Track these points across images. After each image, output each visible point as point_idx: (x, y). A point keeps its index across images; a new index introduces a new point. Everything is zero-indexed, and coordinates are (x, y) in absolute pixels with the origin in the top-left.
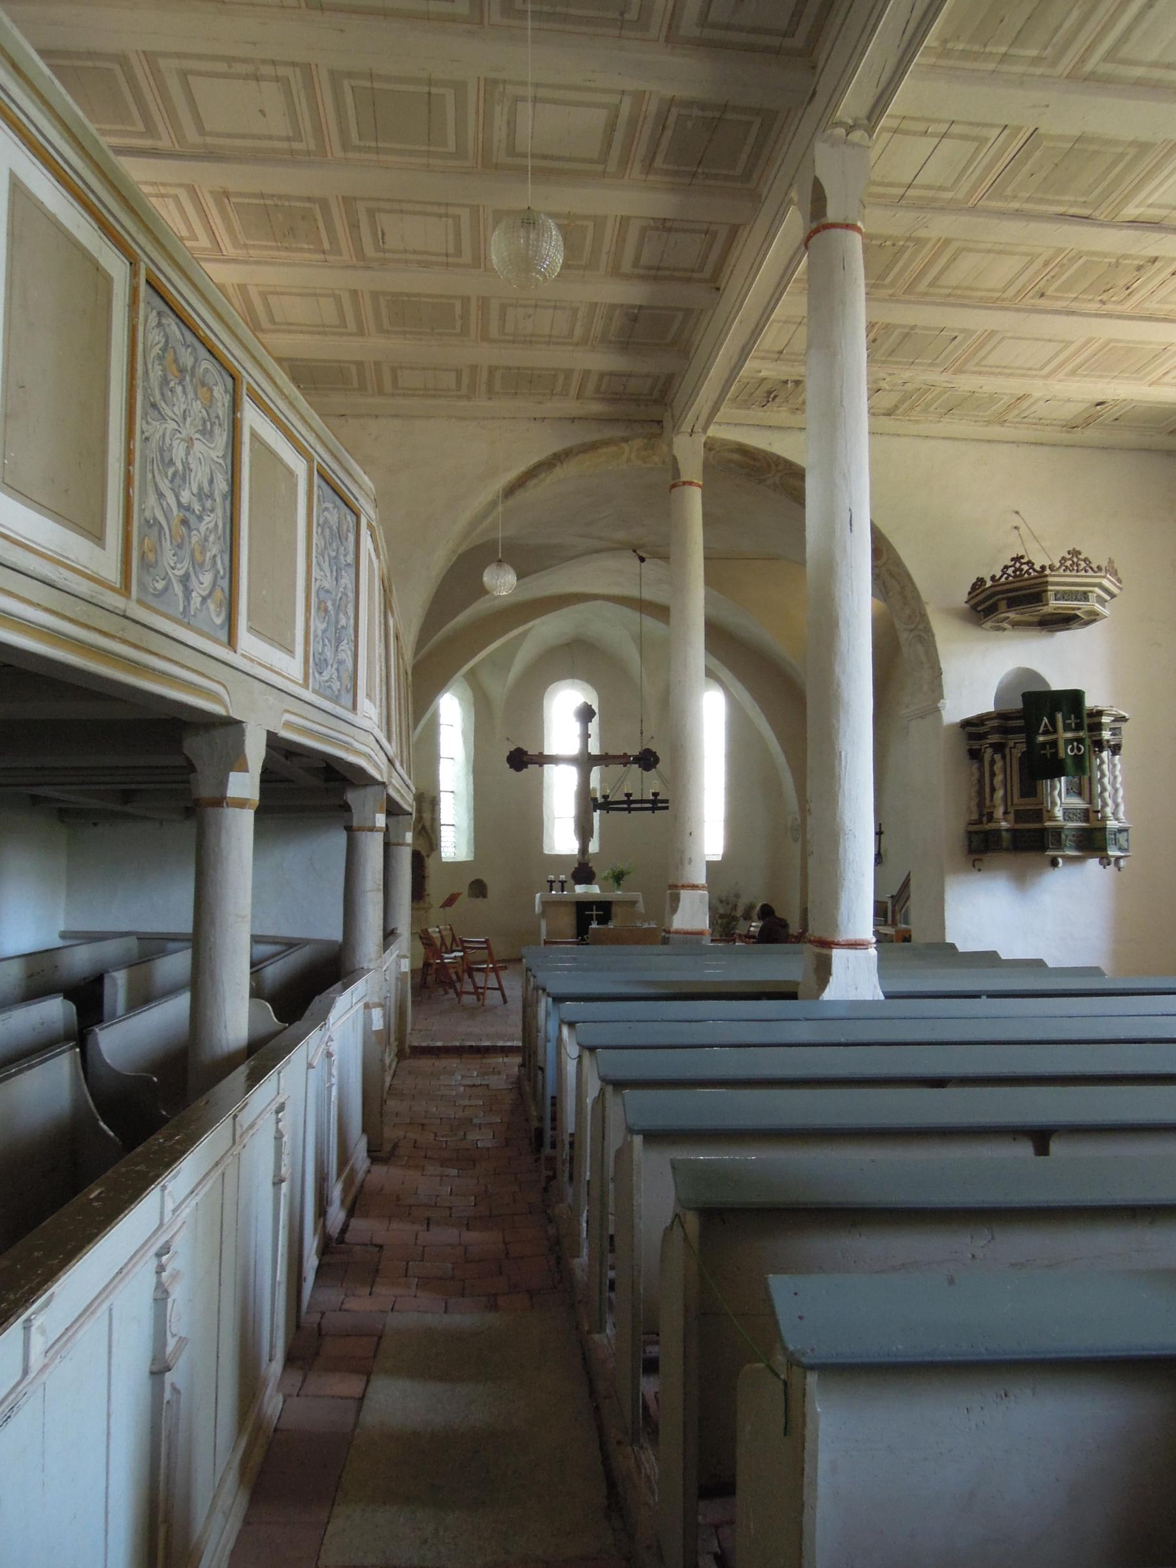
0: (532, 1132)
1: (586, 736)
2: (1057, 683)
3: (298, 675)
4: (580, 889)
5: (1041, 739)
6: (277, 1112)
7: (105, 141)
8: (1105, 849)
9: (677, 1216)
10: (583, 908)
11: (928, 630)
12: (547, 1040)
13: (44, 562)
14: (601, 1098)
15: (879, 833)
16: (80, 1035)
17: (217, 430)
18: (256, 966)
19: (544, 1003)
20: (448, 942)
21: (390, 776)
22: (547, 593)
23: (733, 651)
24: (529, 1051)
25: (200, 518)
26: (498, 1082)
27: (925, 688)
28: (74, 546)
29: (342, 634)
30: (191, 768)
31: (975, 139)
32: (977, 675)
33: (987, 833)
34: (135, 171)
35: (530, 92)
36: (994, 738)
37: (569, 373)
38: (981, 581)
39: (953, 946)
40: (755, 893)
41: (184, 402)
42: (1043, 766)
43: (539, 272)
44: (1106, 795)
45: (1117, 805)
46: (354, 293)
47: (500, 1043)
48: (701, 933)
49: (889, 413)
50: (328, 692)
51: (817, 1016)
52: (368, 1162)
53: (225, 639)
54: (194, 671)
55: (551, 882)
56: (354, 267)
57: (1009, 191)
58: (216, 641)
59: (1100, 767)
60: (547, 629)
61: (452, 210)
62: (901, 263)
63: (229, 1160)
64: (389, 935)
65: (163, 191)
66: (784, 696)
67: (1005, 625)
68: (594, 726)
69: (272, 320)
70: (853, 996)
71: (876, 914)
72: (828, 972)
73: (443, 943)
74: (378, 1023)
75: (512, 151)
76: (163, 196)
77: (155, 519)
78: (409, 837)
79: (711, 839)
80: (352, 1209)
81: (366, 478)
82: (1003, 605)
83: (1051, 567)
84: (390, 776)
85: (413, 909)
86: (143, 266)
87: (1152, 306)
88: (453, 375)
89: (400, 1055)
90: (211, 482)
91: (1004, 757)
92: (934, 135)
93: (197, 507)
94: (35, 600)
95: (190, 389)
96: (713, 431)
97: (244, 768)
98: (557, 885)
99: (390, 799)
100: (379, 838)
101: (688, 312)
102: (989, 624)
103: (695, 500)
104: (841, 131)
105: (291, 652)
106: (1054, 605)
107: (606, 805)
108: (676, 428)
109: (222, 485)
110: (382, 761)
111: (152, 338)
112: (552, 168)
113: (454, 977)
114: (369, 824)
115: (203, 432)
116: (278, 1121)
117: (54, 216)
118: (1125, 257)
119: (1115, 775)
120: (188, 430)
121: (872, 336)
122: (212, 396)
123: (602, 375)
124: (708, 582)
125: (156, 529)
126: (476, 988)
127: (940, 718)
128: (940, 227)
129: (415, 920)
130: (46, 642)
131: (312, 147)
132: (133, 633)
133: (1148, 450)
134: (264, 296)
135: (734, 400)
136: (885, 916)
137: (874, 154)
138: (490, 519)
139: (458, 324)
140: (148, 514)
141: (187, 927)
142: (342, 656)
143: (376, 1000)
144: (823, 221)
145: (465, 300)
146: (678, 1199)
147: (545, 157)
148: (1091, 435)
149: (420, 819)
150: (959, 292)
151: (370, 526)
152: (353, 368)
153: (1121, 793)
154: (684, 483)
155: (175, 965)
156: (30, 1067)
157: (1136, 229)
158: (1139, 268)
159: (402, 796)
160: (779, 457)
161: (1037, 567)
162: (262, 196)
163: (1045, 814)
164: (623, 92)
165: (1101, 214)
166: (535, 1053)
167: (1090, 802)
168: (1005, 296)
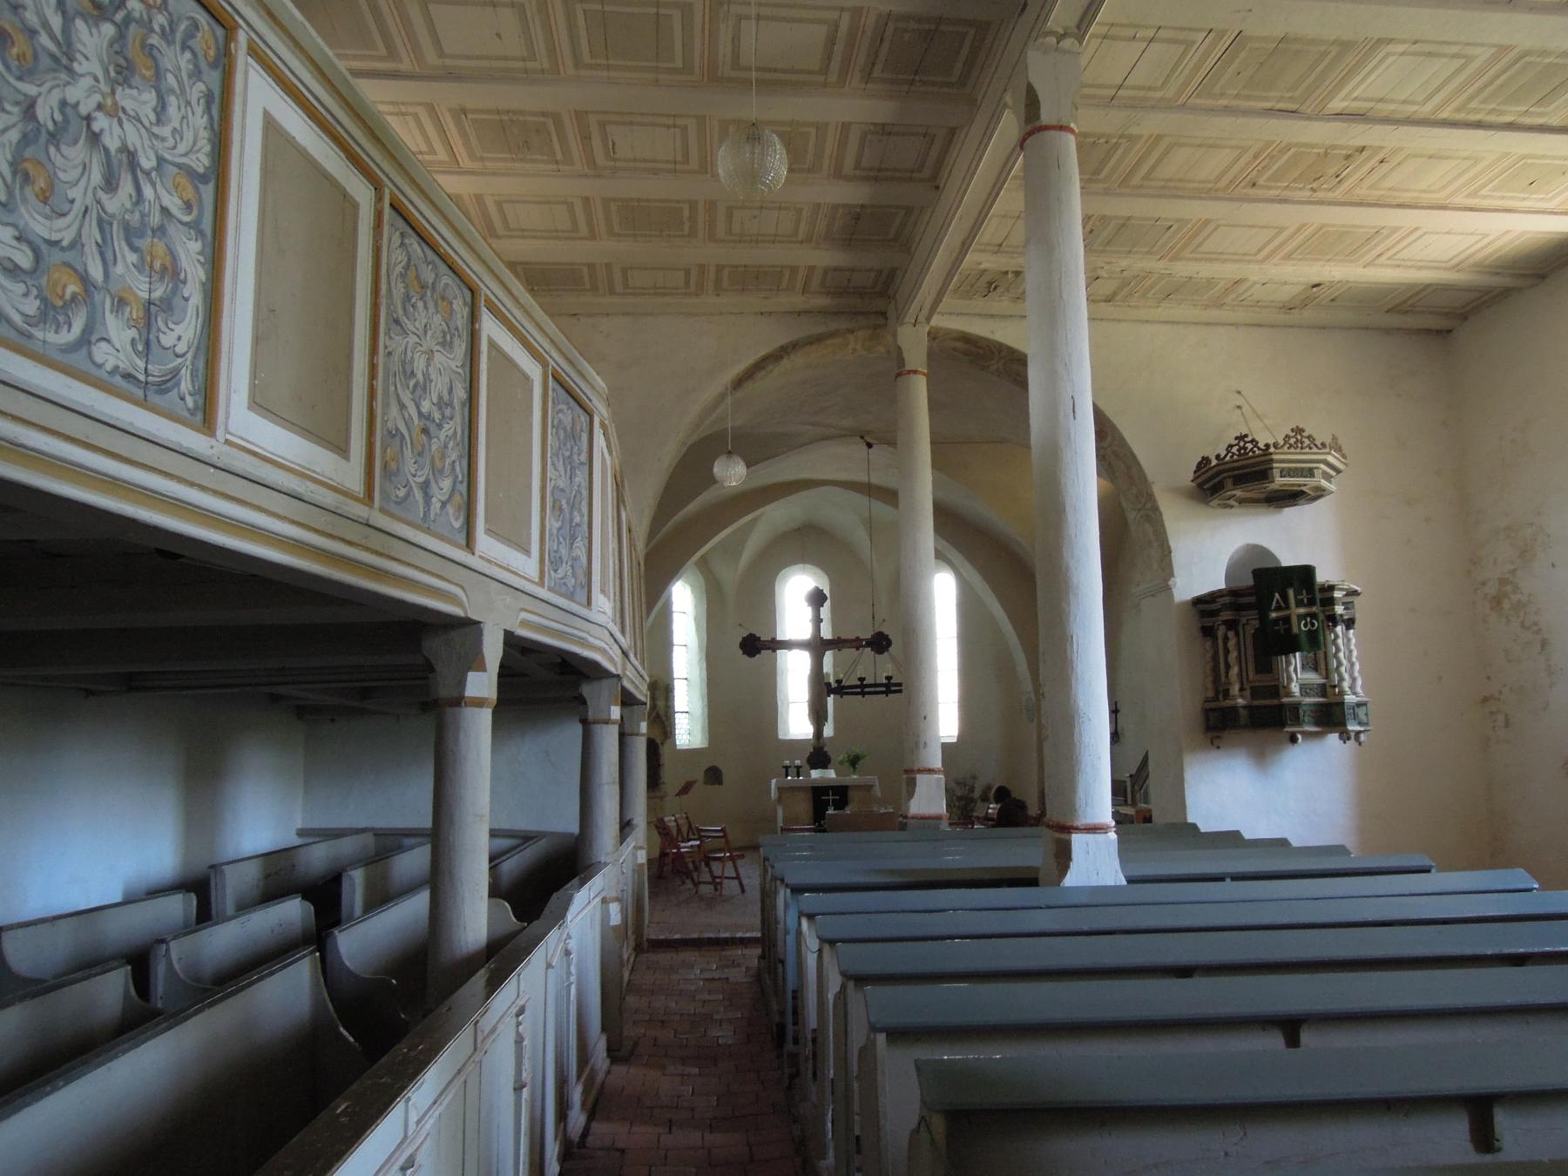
0: (771, 1025)
1: (817, 621)
2: (1288, 558)
3: (535, 575)
4: (815, 774)
5: (1274, 615)
6: (518, 1015)
7: (342, 65)
8: (1344, 724)
9: (922, 1118)
10: (820, 796)
11: (1156, 509)
12: (787, 933)
13: (291, 476)
14: (842, 994)
15: (1114, 711)
16: (318, 937)
17: (457, 342)
18: (495, 859)
19: (783, 895)
20: (684, 830)
21: (624, 669)
22: (775, 480)
23: (963, 535)
24: (768, 941)
25: (440, 426)
26: (737, 975)
27: (1155, 566)
28: (320, 459)
29: (576, 532)
30: (430, 668)
31: (1181, 42)
32: (1206, 553)
33: (1222, 709)
34: (372, 92)
35: (753, 11)
36: (1226, 615)
37: (794, 270)
38: (1206, 460)
39: (1194, 826)
40: (991, 774)
41: (426, 317)
42: (1276, 642)
43: (764, 184)
44: (1343, 669)
45: (1354, 680)
46: (586, 201)
47: (739, 935)
48: (939, 818)
49: (1108, 300)
50: (563, 589)
51: (1061, 903)
52: (608, 1061)
53: (464, 542)
54: (433, 575)
55: (787, 768)
56: (586, 176)
57: (1217, 90)
58: (458, 546)
59: (1334, 642)
60: (778, 515)
61: (679, 122)
62: (1113, 160)
63: (470, 1067)
64: (625, 826)
65: (403, 109)
66: (1015, 578)
67: (1232, 502)
68: (825, 611)
69: (507, 228)
70: (1095, 881)
71: (1115, 792)
72: (1069, 858)
73: (679, 830)
74: (615, 918)
75: (736, 65)
76: (403, 114)
77: (397, 429)
78: (644, 727)
79: (947, 722)
80: (592, 1114)
81: (599, 379)
82: (1229, 483)
83: (1276, 445)
84: (624, 669)
85: (649, 798)
86: (387, 191)
87: (1362, 192)
88: (682, 274)
89: (638, 948)
90: (451, 390)
91: (1237, 634)
92: (1142, 39)
93: (437, 416)
94: (281, 512)
95: (431, 304)
96: (936, 321)
97: (482, 667)
98: (792, 770)
99: (624, 691)
100: (613, 731)
101: (909, 210)
102: (1216, 502)
103: (920, 389)
104: (1053, 40)
105: (527, 552)
106: (1279, 482)
107: (840, 689)
108: (900, 318)
109: (461, 393)
110: (616, 653)
111: (395, 257)
112: (775, 80)
113: (691, 866)
114: (605, 716)
115: (443, 344)
116: (519, 1024)
117: (305, 149)
118: (1334, 147)
119: (1349, 650)
120: (429, 342)
121: (1088, 228)
122: (452, 310)
123: (826, 271)
124: (935, 466)
125: (398, 439)
126: (714, 877)
127: (1171, 596)
128: (1150, 124)
129: (651, 809)
130: (292, 553)
131: (546, 66)
132: (376, 540)
133: (1366, 328)
134: (499, 204)
135: (955, 291)
136: (1125, 796)
137: (1083, 61)
138: (719, 411)
139: (687, 226)
140: (390, 425)
141: (427, 823)
142: (577, 552)
143: (614, 894)
144: (1037, 124)
145: (693, 205)
146: (923, 1102)
147: (769, 70)
148: (1308, 315)
149: (654, 707)
150: (1172, 184)
151: (603, 425)
152: (585, 269)
153: (1357, 667)
154: (909, 372)
155: (413, 862)
156: (272, 973)
157: (1344, 121)
158: (1348, 157)
159: (637, 687)
160: (1001, 345)
161: (1261, 445)
162: (498, 112)
163: (1282, 692)
164: (842, 9)
165: (1308, 108)
166: (775, 946)
167: (1327, 677)
168: (1219, 185)
